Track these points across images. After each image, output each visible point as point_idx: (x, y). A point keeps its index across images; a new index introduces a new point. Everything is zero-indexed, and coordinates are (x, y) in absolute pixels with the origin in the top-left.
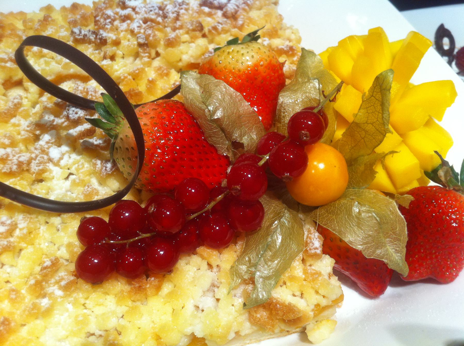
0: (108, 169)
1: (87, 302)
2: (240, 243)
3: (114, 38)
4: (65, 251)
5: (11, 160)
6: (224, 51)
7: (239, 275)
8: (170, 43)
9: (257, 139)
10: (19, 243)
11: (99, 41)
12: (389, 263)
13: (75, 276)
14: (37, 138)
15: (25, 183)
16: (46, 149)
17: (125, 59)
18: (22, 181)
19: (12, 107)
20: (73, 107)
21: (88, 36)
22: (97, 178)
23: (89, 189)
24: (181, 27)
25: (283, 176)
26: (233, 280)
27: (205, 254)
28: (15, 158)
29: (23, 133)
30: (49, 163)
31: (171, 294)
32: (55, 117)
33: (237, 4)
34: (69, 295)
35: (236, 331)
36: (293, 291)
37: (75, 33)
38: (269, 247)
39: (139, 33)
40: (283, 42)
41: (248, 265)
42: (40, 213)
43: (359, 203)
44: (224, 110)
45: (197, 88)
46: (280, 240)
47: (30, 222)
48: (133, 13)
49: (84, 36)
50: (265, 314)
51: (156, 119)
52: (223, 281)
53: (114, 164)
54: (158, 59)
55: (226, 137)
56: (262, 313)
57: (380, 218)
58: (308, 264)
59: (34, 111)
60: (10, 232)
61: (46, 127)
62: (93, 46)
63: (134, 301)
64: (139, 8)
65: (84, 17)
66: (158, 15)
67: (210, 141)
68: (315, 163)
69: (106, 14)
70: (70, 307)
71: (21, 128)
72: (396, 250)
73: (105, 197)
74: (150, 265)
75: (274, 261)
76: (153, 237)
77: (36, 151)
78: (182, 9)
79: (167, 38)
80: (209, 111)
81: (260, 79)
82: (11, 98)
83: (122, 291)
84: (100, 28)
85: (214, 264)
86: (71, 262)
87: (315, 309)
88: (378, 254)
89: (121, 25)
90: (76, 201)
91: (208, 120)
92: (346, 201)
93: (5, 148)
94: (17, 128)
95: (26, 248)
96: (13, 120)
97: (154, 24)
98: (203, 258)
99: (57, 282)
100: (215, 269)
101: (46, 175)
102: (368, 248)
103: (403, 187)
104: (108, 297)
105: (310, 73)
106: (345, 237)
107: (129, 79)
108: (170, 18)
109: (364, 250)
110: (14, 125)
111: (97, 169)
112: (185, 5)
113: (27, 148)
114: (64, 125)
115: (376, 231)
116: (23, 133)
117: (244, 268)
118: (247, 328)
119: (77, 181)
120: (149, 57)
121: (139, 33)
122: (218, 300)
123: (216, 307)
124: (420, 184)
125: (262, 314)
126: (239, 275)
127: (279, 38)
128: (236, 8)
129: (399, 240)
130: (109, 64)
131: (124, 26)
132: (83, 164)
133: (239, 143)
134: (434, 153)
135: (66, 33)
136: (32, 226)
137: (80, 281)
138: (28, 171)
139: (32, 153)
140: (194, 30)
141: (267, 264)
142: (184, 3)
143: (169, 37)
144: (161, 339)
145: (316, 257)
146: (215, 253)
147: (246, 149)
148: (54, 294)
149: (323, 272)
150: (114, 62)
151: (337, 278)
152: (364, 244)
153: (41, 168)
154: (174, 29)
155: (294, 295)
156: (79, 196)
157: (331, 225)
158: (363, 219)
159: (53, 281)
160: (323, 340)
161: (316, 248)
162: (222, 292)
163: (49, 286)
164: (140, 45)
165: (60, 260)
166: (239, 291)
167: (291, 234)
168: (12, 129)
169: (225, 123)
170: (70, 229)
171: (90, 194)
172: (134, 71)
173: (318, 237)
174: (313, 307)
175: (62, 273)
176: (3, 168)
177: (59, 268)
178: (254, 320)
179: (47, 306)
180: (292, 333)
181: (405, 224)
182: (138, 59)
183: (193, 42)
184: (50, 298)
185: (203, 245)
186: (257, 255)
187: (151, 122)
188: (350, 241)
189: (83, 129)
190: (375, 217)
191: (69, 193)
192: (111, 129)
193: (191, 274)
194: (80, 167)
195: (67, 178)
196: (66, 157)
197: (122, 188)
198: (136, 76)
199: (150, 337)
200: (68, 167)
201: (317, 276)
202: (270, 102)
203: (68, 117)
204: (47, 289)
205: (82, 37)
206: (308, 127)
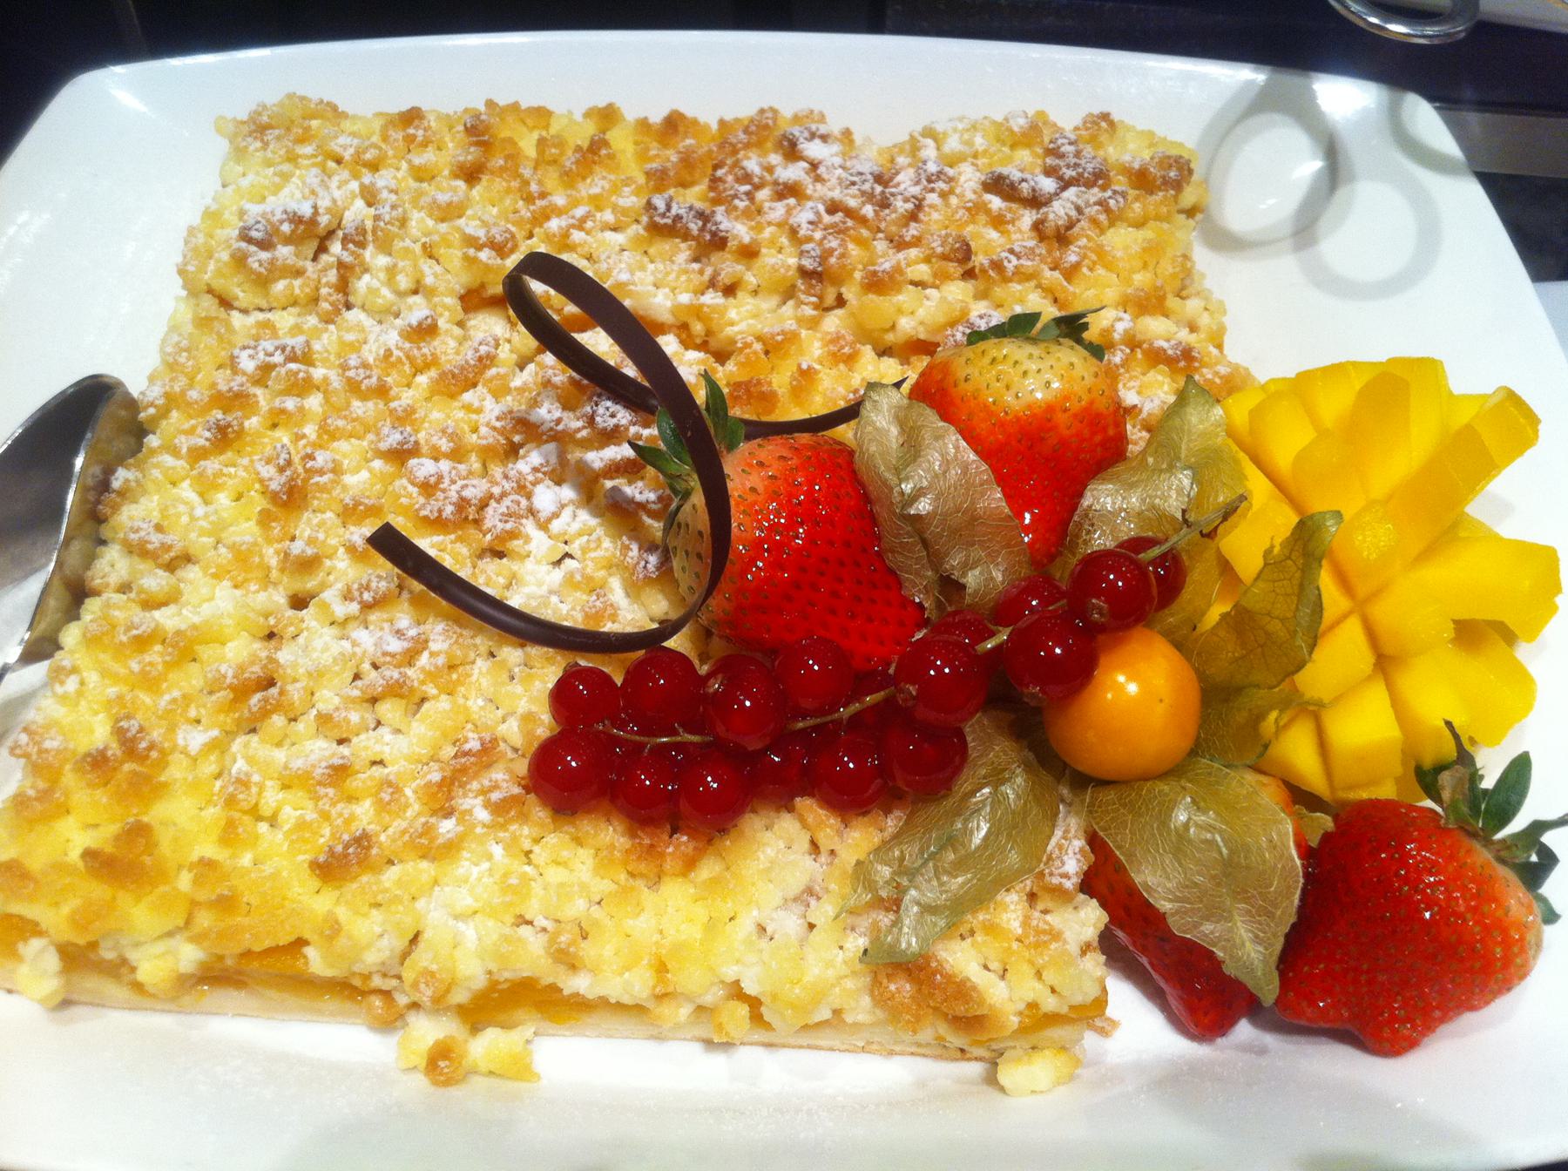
0: (649, 566)
1: (536, 849)
2: (897, 813)
3: (747, 240)
4: (516, 729)
5: (444, 491)
6: (983, 352)
7: (870, 885)
8: (878, 284)
9: (1003, 583)
10: (423, 683)
11: (708, 237)
12: (1228, 961)
13: (524, 787)
14: (512, 451)
15: (464, 550)
16: (528, 484)
17: (760, 295)
18: (458, 545)
19: (472, 362)
20: (609, 399)
21: (684, 221)
22: (624, 580)
23: (598, 604)
24: (917, 242)
25: (1025, 691)
26: (855, 892)
27: (810, 819)
28: (454, 487)
29: (484, 430)
30: (527, 518)
31: (715, 882)
32: (565, 408)
33: (1080, 202)
34: (503, 827)
35: (837, 1006)
36: (986, 958)
37: (656, 209)
38: (951, 842)
39: (809, 239)
40: (1174, 328)
41: (896, 868)
42: (480, 631)
43: (1194, 801)
44: (937, 498)
45: (894, 431)
46: (983, 833)
47: (456, 642)
48: (807, 180)
49: (674, 221)
50: (908, 987)
51: (780, 482)
52: (833, 886)
53: (665, 560)
54: (839, 312)
55: (930, 561)
56: (902, 982)
57: (1232, 852)
58: (1040, 906)
59: (518, 381)
60: (410, 657)
61: (540, 431)
62: (690, 246)
63: (632, 875)
64: (827, 168)
65: (687, 161)
66: (869, 197)
67: (891, 560)
68: (1121, 678)
69: (743, 168)
70: (497, 851)
71: (482, 419)
72: (1257, 936)
73: (629, 629)
74: (684, 806)
75: (956, 877)
76: (707, 744)
77: (504, 482)
78: (932, 190)
79: (872, 268)
80: (902, 493)
81: (1052, 440)
82: (478, 335)
83: (612, 847)
84: (717, 201)
85: (825, 845)
86: (523, 756)
87: (1027, 1012)
88: (1207, 932)
89: (770, 208)
90: (566, 623)
91: (894, 513)
92: (1166, 789)
93: (436, 459)
94: (474, 416)
95: (435, 697)
96: (468, 396)
97: (850, 223)
98: (805, 825)
99: (484, 792)
100: (823, 858)
101: (516, 544)
102: (1185, 913)
103: (1351, 787)
104: (581, 851)
105: (1183, 447)
106: (1139, 871)
107: (755, 353)
108: (895, 211)
109: (1173, 915)
110: (468, 408)
111: (628, 559)
112: (945, 182)
113: (485, 466)
114: (579, 436)
115: (1213, 877)
116: (484, 430)
117: (885, 871)
118: (862, 1009)
119: (578, 577)
120: (816, 307)
121: (809, 239)
122: (811, 926)
123: (802, 942)
124: (1399, 792)
125: (902, 988)
126: (870, 885)
127: (1167, 316)
128: (1073, 213)
129: (1271, 915)
130: (718, 305)
131: (778, 211)
132: (599, 539)
133: (957, 583)
134: (1443, 724)
135: (634, 199)
136: (459, 653)
137: (532, 797)
138: (477, 522)
139: (494, 483)
140: (944, 257)
141: (938, 879)
142: (942, 177)
143: (877, 268)
144: (667, 971)
145: (1059, 893)
146: (833, 821)
147: (968, 600)
148: (471, 815)
149: (1068, 935)
150: (731, 300)
151: (1103, 958)
152: (1177, 900)
153: (509, 526)
154: (900, 244)
155: (986, 967)
156: (574, 613)
157: (1117, 834)
158: (1190, 841)
159: (475, 785)
160: (1033, 1092)
161: (1066, 876)
162: (823, 911)
163: (465, 796)
164: (804, 273)
165: (501, 744)
166: (864, 923)
167: (1014, 828)
168: (460, 414)
169: (933, 529)
170: (537, 683)
171: (598, 616)
172: (773, 336)
173: (1081, 850)
174: (1022, 1006)
175: (498, 775)
176: (423, 506)
177: (495, 762)
178: (881, 995)
179: (450, 836)
180: (969, 1059)
181: (1297, 882)
182: (791, 303)
183: (937, 287)
184: (460, 821)
185: (812, 795)
186: (922, 852)
187: (766, 488)
188: (1146, 883)
189: (619, 457)
190: (1218, 845)
191: (554, 599)
192: (679, 476)
193: (770, 852)
194: (593, 545)
195: (559, 562)
196: (567, 514)
197: (674, 615)
198: (774, 347)
199: (645, 962)
200: (566, 538)
201: (1046, 938)
202: (1066, 500)
203: (591, 421)
204: (460, 801)
205: (669, 221)
206: (1111, 593)
